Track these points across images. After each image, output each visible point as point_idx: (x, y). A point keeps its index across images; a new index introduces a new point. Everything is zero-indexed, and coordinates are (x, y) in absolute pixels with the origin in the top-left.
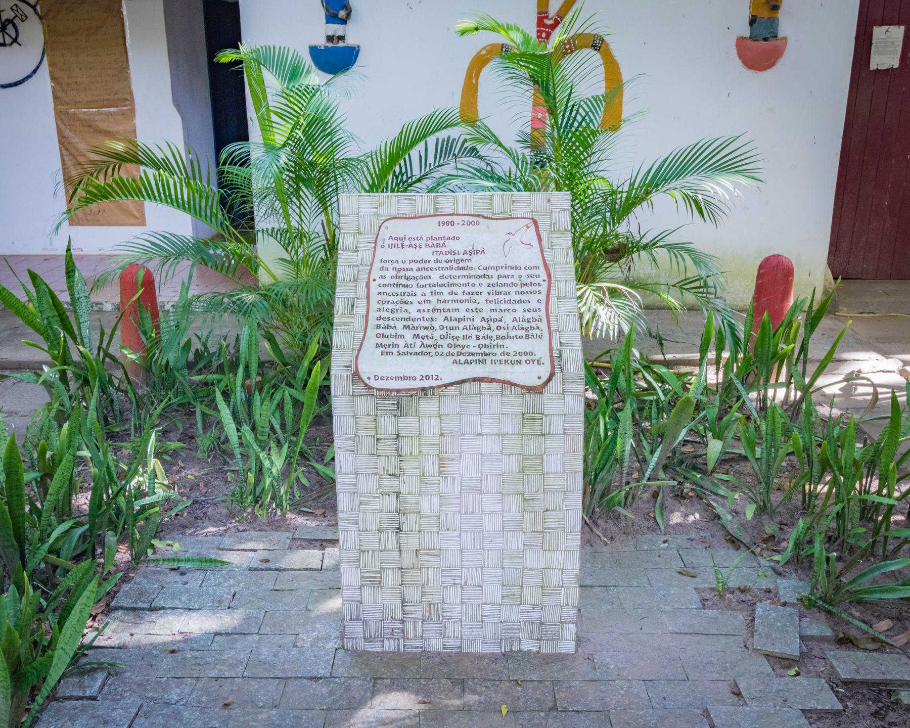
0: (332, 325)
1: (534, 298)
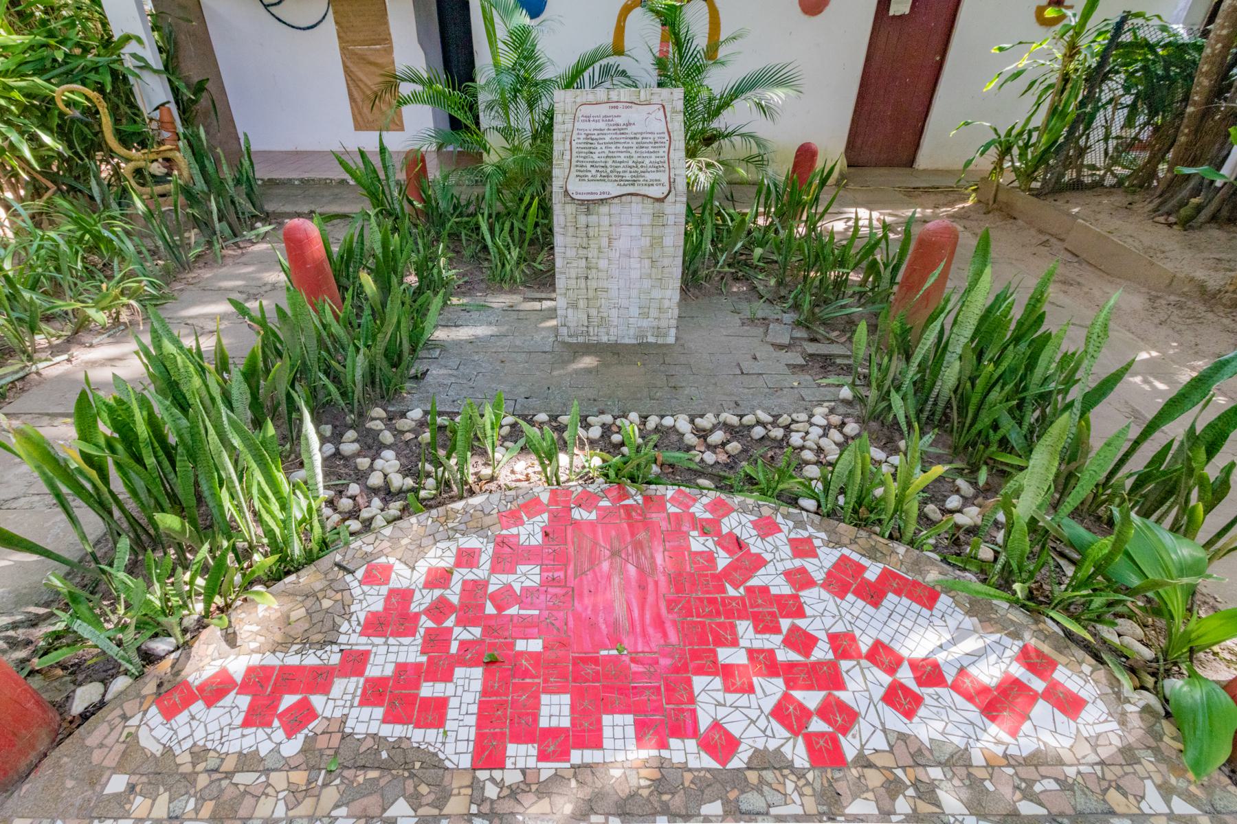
1: (661, 150)
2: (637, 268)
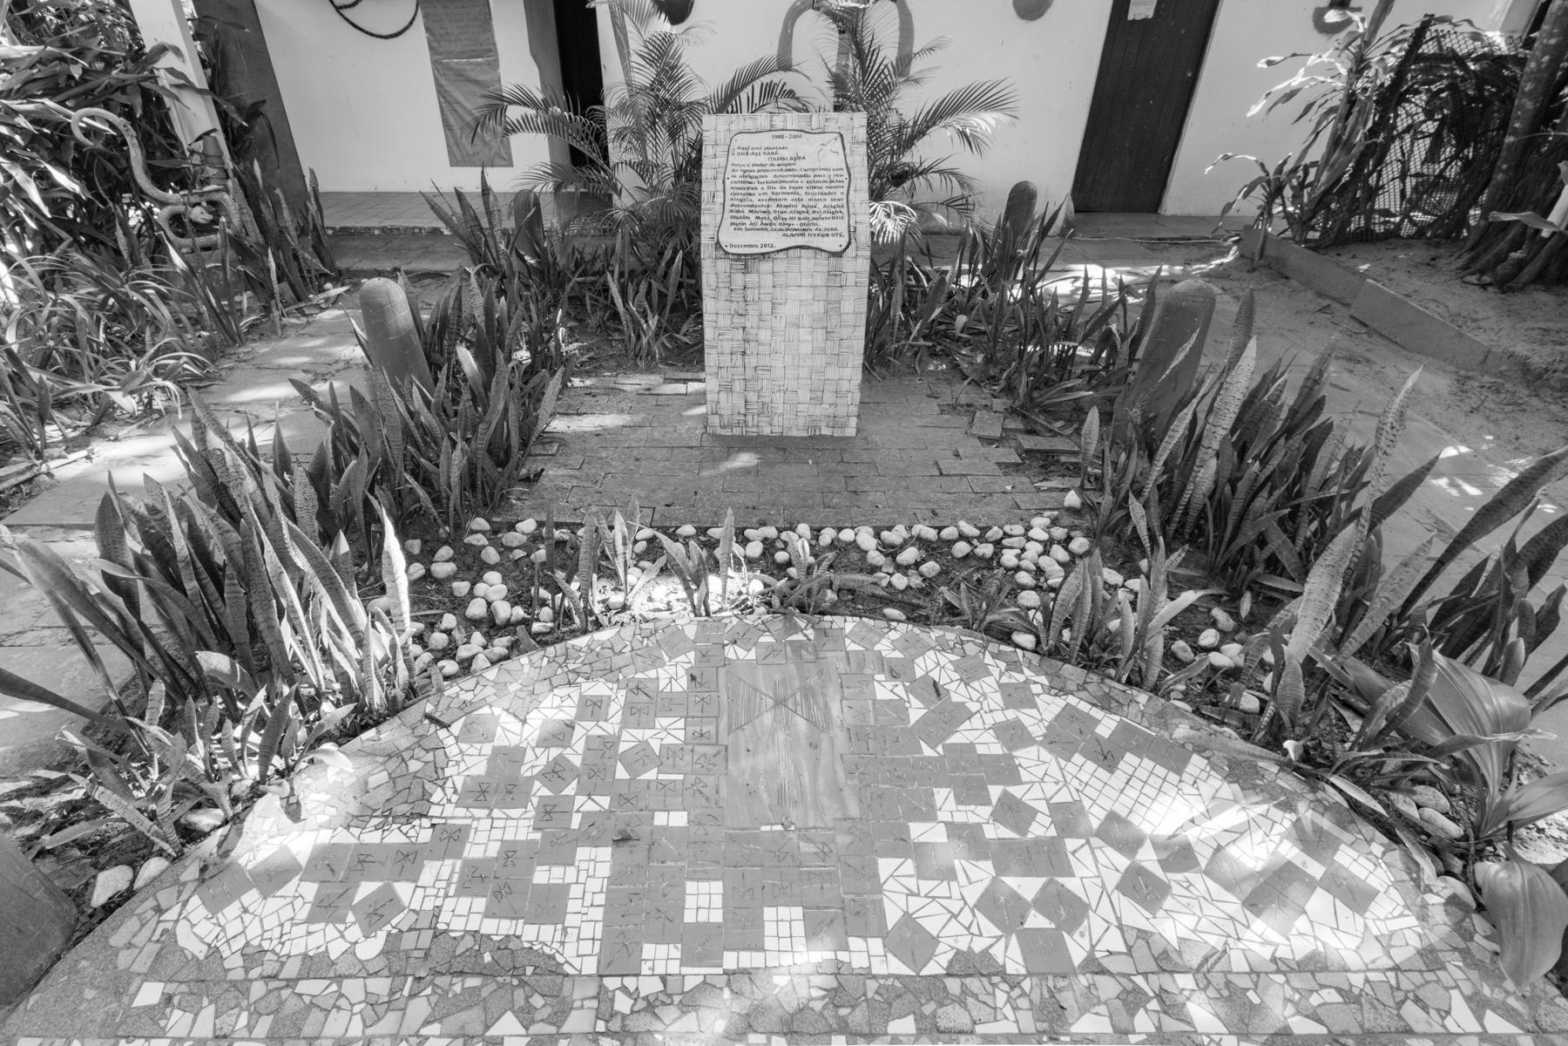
0: (699, 208)
2: (807, 340)
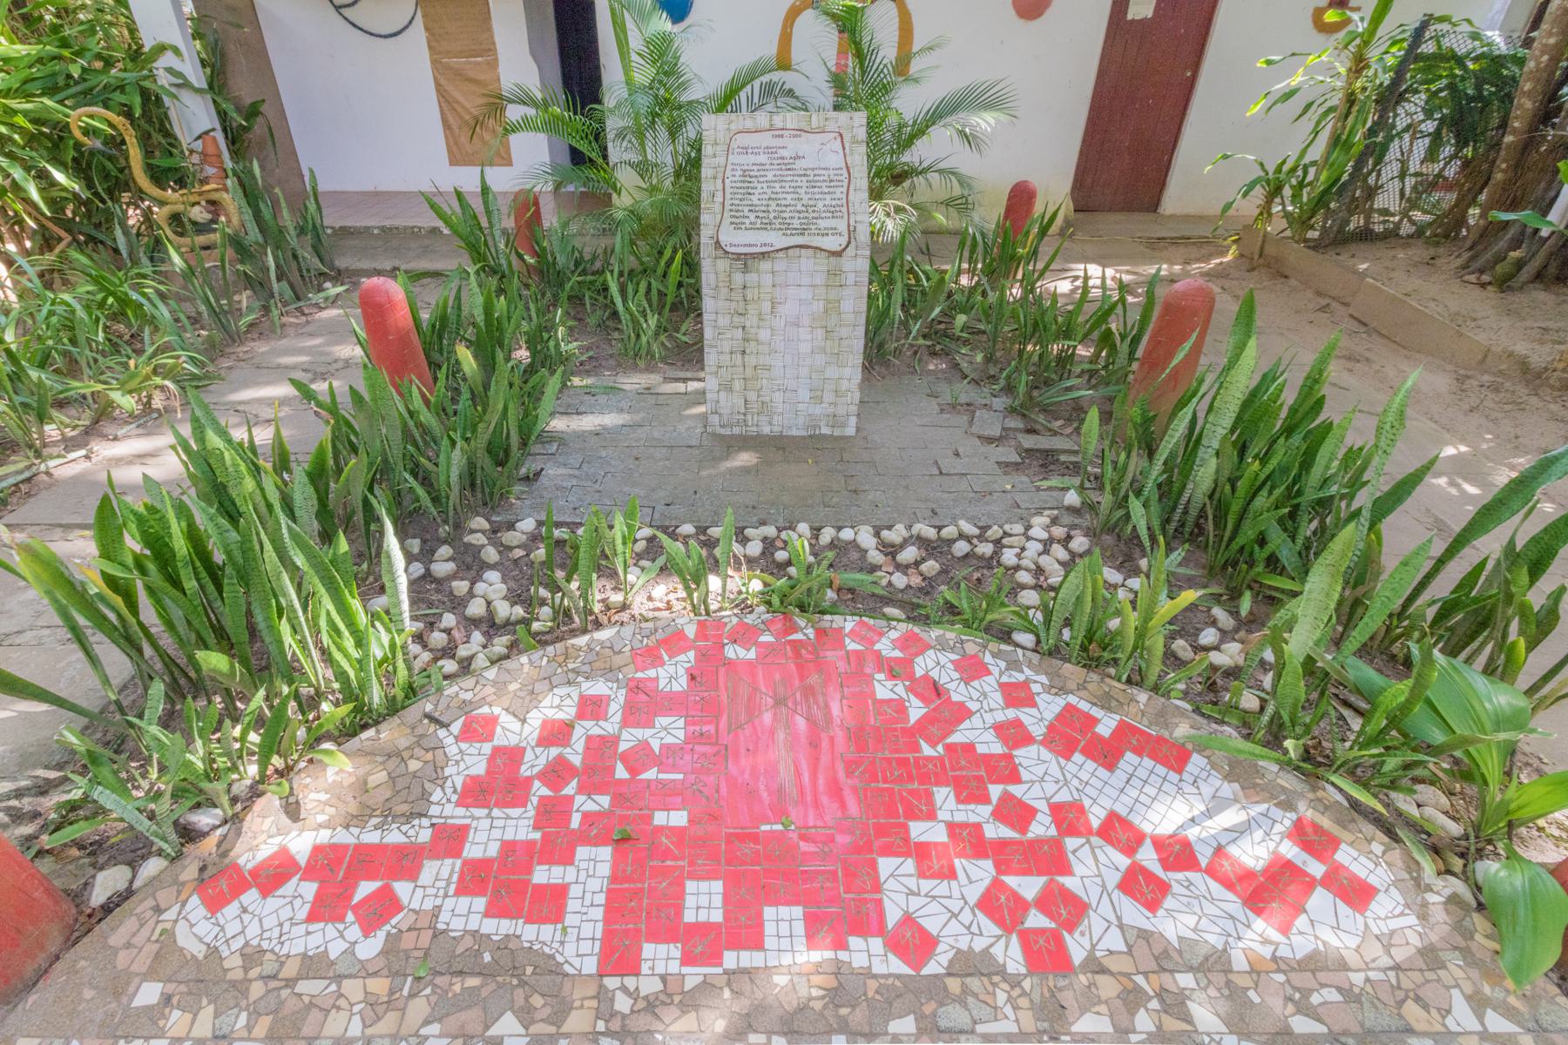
1: (838, 190)
2: (807, 340)
